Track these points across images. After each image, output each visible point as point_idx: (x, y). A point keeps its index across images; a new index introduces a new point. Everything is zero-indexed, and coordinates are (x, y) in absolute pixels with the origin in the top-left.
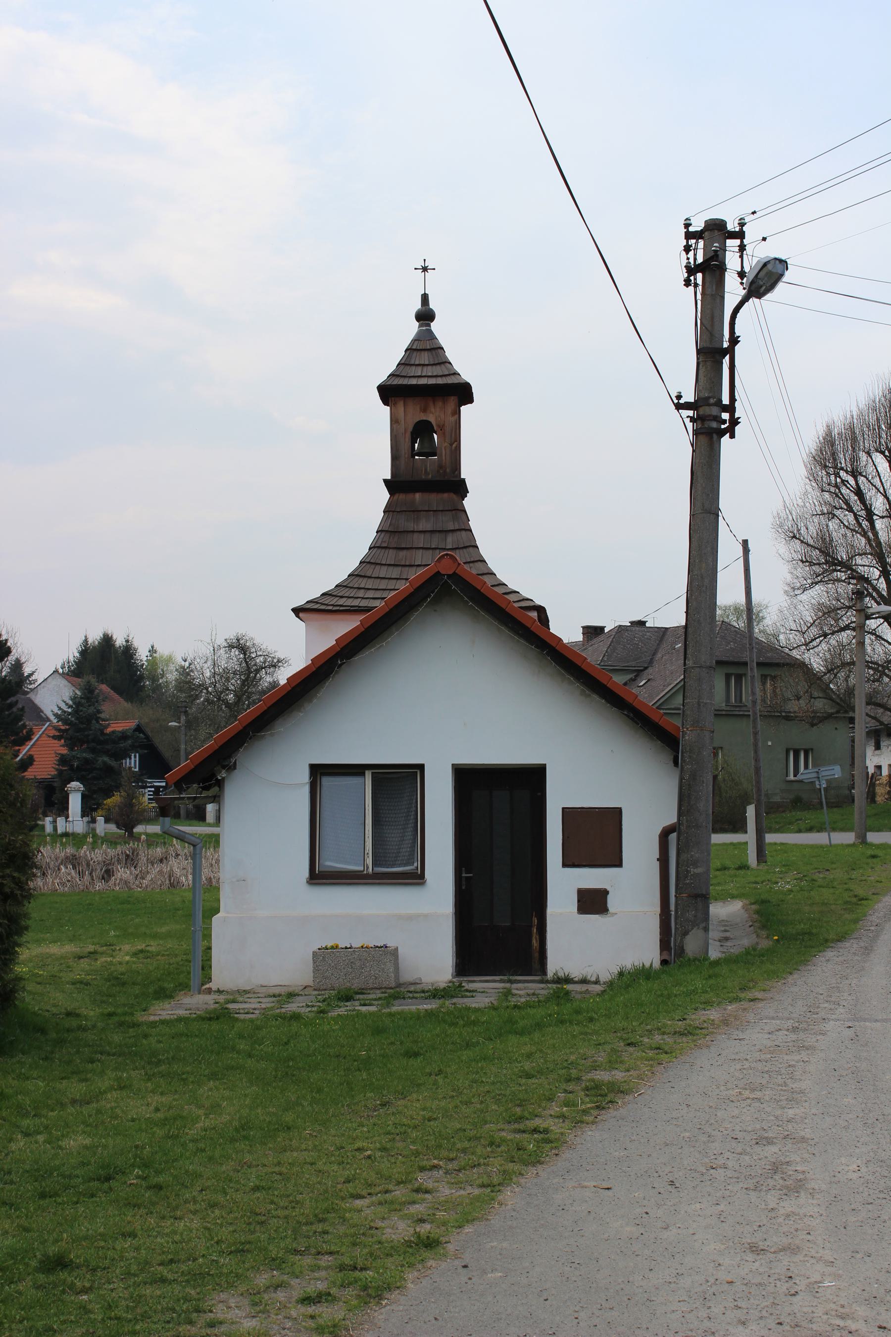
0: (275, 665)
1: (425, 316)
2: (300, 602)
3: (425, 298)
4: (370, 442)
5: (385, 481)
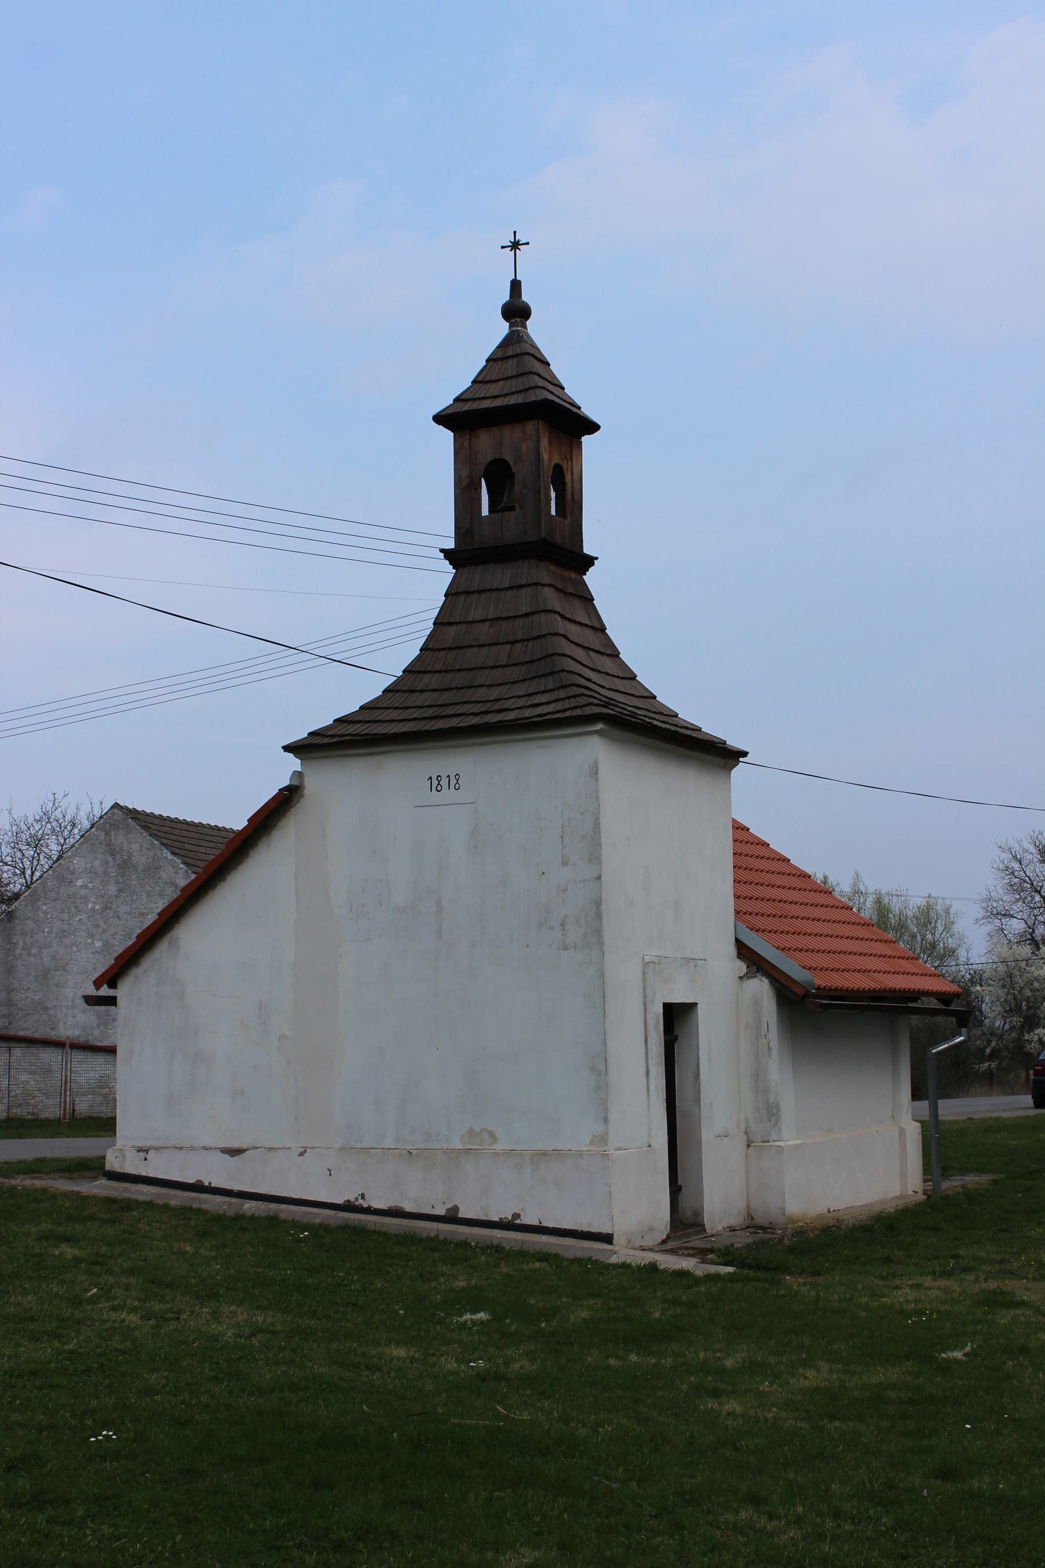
1: (516, 311)
2: (300, 734)
3: (516, 286)
4: (423, 492)
5: (447, 554)
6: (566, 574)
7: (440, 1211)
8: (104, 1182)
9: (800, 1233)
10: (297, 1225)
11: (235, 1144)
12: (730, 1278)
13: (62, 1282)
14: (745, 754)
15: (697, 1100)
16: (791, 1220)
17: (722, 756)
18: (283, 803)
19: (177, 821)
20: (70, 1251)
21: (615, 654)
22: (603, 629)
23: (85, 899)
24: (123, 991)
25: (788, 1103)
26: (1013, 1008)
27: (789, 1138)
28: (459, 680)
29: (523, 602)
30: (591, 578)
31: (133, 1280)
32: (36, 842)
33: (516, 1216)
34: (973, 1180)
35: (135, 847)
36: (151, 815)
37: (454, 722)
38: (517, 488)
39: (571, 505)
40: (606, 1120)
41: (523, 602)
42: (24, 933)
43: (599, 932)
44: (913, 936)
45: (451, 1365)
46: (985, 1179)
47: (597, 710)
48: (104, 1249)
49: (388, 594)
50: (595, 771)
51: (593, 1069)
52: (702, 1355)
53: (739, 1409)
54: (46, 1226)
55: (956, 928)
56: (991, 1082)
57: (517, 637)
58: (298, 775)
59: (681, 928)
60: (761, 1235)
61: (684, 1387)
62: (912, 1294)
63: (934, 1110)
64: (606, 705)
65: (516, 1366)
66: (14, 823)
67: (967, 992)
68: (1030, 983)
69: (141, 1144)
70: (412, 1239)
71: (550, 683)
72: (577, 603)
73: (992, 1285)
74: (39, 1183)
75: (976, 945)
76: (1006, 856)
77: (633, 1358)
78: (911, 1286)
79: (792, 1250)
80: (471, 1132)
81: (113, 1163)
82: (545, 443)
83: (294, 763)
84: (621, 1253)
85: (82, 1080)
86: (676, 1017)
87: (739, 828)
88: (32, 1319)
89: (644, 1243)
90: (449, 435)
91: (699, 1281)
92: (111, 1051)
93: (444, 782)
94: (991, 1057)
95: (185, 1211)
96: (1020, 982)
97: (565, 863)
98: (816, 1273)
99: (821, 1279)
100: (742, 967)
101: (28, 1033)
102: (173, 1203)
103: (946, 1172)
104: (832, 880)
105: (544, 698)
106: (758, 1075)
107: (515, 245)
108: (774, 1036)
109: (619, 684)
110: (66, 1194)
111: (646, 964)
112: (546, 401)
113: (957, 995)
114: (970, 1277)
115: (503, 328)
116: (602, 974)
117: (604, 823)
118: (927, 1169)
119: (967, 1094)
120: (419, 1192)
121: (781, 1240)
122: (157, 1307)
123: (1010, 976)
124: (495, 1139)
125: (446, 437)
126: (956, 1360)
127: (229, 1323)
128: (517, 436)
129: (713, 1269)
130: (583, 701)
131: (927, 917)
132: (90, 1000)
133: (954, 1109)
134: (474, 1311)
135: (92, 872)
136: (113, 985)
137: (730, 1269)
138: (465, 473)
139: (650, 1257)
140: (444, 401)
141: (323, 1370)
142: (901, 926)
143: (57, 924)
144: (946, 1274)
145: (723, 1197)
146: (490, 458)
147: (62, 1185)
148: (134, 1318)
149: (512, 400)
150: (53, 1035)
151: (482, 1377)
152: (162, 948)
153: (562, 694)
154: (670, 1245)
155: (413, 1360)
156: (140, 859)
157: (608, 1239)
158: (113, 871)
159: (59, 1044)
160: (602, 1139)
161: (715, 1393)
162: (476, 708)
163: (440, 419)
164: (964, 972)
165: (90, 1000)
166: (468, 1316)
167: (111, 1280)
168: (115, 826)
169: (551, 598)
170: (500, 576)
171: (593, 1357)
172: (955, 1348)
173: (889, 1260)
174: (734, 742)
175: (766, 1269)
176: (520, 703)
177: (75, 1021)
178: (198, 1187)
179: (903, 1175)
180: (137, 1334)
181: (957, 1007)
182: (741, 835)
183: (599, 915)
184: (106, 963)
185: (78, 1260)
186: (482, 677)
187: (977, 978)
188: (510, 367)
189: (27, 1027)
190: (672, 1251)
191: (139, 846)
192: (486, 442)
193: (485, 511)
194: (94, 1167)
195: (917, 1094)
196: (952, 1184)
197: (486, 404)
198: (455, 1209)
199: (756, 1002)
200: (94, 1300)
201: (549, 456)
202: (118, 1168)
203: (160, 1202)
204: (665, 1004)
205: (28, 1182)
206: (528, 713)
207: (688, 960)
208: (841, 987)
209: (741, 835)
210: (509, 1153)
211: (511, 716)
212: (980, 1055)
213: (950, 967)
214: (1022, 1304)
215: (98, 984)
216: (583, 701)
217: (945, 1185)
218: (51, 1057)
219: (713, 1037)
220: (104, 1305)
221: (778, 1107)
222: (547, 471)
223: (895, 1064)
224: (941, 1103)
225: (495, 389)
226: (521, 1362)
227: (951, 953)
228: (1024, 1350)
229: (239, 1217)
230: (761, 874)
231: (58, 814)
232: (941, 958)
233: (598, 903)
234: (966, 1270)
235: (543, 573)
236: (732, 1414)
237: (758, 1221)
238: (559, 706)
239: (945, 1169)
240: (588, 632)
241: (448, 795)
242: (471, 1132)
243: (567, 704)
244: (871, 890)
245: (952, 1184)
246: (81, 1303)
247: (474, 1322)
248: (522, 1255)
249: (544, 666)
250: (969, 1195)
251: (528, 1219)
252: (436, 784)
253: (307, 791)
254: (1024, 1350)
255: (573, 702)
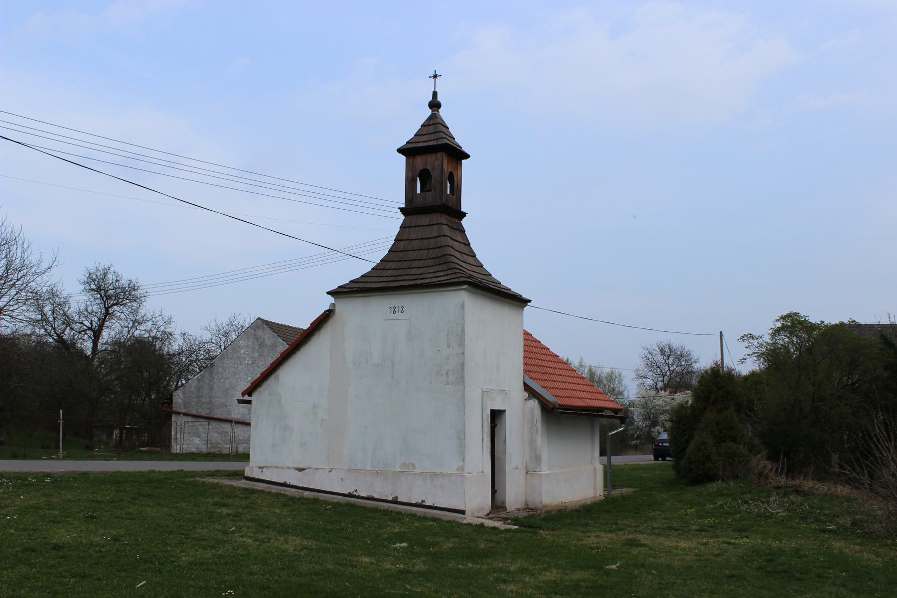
0: (687, 402)
1: (435, 105)
2: (334, 287)
3: (435, 94)
4: (391, 182)
5: (401, 209)
6: (453, 220)
7: (390, 498)
8: (244, 481)
9: (548, 512)
10: (326, 502)
11: (301, 466)
12: (516, 531)
13: (220, 524)
14: (530, 301)
15: (505, 452)
16: (545, 506)
17: (520, 302)
18: (327, 316)
19: (285, 326)
20: (225, 511)
21: (474, 256)
22: (469, 245)
23: (244, 359)
24: (254, 398)
25: (545, 456)
26: (647, 417)
27: (545, 470)
28: (404, 265)
29: (434, 232)
30: (464, 222)
31: (251, 524)
32: (226, 334)
33: (423, 501)
34: (625, 491)
35: (267, 337)
36: (274, 323)
37: (402, 283)
38: (433, 181)
39: (457, 190)
40: (464, 460)
41: (434, 232)
42: (218, 373)
43: (463, 377)
44: (605, 385)
45: (389, 566)
46: (631, 490)
47: (464, 279)
48: (240, 510)
49: (375, 228)
50: (463, 306)
51: (458, 437)
52: (500, 565)
53: (514, 589)
54: (216, 499)
55: (623, 382)
56: (637, 449)
57: (430, 248)
58: (333, 305)
59: (499, 378)
60: (531, 512)
61: (491, 579)
62: (595, 540)
63: (609, 460)
64: (469, 277)
65: (417, 567)
66: (217, 326)
67: (627, 411)
68: (654, 407)
69: (260, 465)
70: (376, 510)
71: (444, 267)
72: (458, 233)
73: (631, 537)
74: (215, 481)
75: (632, 390)
76: (646, 352)
77: (470, 565)
78: (595, 536)
79: (544, 519)
80: (404, 464)
81: (248, 473)
82: (445, 162)
83: (331, 300)
84: (469, 519)
85: (241, 437)
86: (496, 416)
87: (527, 334)
88: (205, 540)
89: (479, 515)
90: (404, 158)
91: (502, 532)
92: (249, 424)
93: (397, 310)
94: (637, 438)
95: (278, 495)
96: (650, 406)
97: (449, 347)
98: (554, 530)
99: (556, 533)
100: (526, 395)
101: (218, 416)
102: (273, 491)
103: (614, 487)
104: (570, 360)
105: (441, 274)
106: (532, 442)
107: (435, 76)
108: (539, 425)
109: (475, 269)
110: (226, 486)
111: (483, 392)
112: (446, 144)
113: (621, 410)
114: (621, 533)
115: (429, 112)
116: (464, 396)
117: (467, 329)
118: (605, 486)
119: (626, 454)
120: (381, 490)
121: (540, 515)
122: (261, 536)
123: (646, 403)
124: (415, 468)
125: (403, 158)
126: (612, 569)
127: (292, 544)
128: (434, 160)
129: (508, 527)
130: (458, 275)
131: (611, 377)
132: (241, 402)
133: (618, 460)
134: (401, 543)
135: (248, 347)
136: (250, 395)
137: (516, 527)
138: (410, 174)
139: (478, 521)
140: (402, 143)
141: (331, 567)
142: (600, 381)
143: (232, 369)
144: (611, 531)
145: (515, 496)
146: (421, 168)
147: (226, 482)
148: (250, 541)
149: (432, 143)
150: (229, 417)
151: (402, 572)
152: (272, 379)
153: (449, 272)
154: (490, 516)
155: (371, 563)
156: (269, 342)
157: (463, 512)
158: (257, 347)
159: (230, 421)
160: (462, 468)
161: (505, 582)
162: (412, 277)
163: (400, 151)
164: (626, 401)
165: (241, 402)
166: (398, 545)
167: (242, 524)
168: (258, 327)
169: (446, 230)
170: (424, 220)
171: (452, 565)
172: (613, 564)
173: (587, 525)
174: (525, 296)
175: (532, 527)
176: (431, 275)
177: (238, 412)
178: (285, 485)
179: (595, 488)
180: (250, 548)
181: (621, 415)
182: (528, 337)
183: (463, 369)
184: (246, 385)
185: (228, 515)
186: (415, 264)
187: (632, 404)
188: (431, 129)
189: (218, 414)
190: (491, 519)
191: (268, 336)
192: (420, 162)
193: (419, 191)
194: (240, 475)
195: (602, 453)
196: (616, 492)
197: (420, 145)
198: (396, 497)
199: (532, 410)
200: (233, 532)
201: (447, 168)
202: (250, 476)
203: (267, 490)
204: (492, 411)
205: (211, 480)
206: (434, 280)
207: (502, 391)
208: (569, 406)
209: (528, 337)
210: (420, 474)
211: (427, 281)
212: (632, 438)
213: (620, 399)
214: (644, 545)
215: (243, 394)
216: (458, 275)
217: (613, 493)
218: (227, 426)
219: (512, 425)
220: (237, 535)
221: (540, 457)
222: (446, 175)
223: (593, 440)
224: (613, 458)
225: (425, 138)
226: (420, 566)
227: (621, 393)
228: (643, 565)
229: (301, 498)
230: (535, 353)
231: (236, 322)
232: (617, 395)
233: (463, 365)
234: (620, 530)
235: (443, 219)
236: (511, 591)
237: (531, 506)
238: (448, 277)
239: (613, 486)
240: (462, 246)
241: (398, 315)
242: (404, 464)
243: (451, 276)
244: (587, 364)
245: (616, 492)
246: (227, 534)
247: (401, 547)
248: (425, 518)
249: (443, 260)
250: (623, 498)
251: (428, 503)
252: (393, 310)
253: (337, 312)
254: (643, 565)
255: (454, 276)
